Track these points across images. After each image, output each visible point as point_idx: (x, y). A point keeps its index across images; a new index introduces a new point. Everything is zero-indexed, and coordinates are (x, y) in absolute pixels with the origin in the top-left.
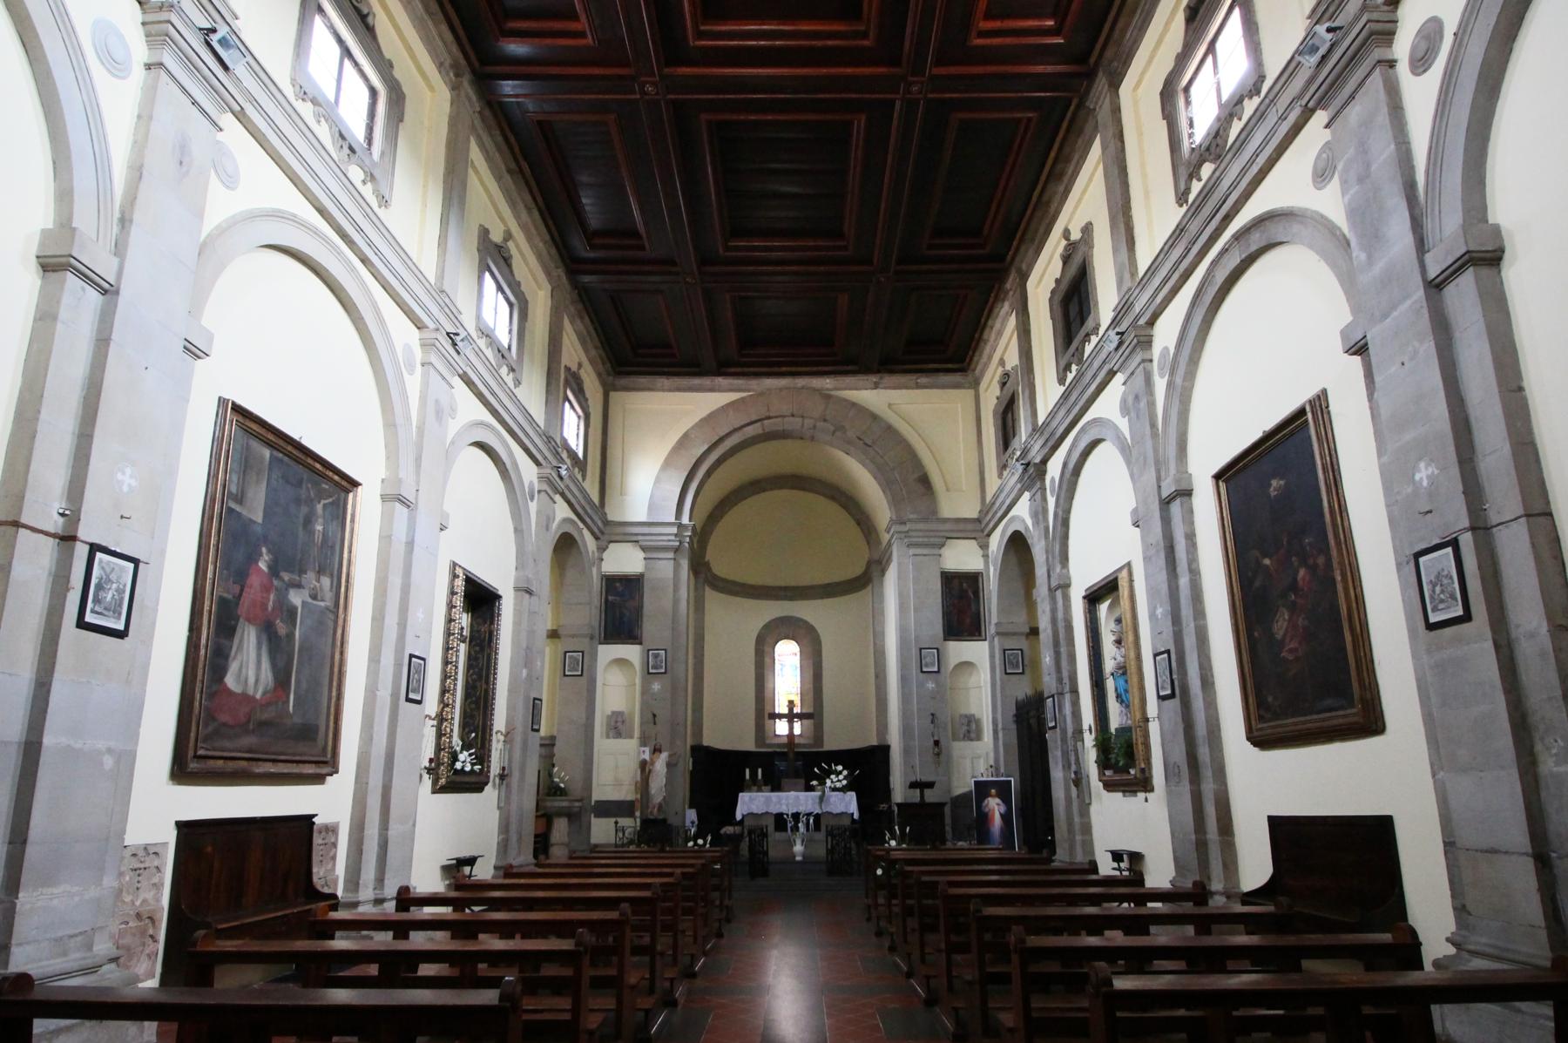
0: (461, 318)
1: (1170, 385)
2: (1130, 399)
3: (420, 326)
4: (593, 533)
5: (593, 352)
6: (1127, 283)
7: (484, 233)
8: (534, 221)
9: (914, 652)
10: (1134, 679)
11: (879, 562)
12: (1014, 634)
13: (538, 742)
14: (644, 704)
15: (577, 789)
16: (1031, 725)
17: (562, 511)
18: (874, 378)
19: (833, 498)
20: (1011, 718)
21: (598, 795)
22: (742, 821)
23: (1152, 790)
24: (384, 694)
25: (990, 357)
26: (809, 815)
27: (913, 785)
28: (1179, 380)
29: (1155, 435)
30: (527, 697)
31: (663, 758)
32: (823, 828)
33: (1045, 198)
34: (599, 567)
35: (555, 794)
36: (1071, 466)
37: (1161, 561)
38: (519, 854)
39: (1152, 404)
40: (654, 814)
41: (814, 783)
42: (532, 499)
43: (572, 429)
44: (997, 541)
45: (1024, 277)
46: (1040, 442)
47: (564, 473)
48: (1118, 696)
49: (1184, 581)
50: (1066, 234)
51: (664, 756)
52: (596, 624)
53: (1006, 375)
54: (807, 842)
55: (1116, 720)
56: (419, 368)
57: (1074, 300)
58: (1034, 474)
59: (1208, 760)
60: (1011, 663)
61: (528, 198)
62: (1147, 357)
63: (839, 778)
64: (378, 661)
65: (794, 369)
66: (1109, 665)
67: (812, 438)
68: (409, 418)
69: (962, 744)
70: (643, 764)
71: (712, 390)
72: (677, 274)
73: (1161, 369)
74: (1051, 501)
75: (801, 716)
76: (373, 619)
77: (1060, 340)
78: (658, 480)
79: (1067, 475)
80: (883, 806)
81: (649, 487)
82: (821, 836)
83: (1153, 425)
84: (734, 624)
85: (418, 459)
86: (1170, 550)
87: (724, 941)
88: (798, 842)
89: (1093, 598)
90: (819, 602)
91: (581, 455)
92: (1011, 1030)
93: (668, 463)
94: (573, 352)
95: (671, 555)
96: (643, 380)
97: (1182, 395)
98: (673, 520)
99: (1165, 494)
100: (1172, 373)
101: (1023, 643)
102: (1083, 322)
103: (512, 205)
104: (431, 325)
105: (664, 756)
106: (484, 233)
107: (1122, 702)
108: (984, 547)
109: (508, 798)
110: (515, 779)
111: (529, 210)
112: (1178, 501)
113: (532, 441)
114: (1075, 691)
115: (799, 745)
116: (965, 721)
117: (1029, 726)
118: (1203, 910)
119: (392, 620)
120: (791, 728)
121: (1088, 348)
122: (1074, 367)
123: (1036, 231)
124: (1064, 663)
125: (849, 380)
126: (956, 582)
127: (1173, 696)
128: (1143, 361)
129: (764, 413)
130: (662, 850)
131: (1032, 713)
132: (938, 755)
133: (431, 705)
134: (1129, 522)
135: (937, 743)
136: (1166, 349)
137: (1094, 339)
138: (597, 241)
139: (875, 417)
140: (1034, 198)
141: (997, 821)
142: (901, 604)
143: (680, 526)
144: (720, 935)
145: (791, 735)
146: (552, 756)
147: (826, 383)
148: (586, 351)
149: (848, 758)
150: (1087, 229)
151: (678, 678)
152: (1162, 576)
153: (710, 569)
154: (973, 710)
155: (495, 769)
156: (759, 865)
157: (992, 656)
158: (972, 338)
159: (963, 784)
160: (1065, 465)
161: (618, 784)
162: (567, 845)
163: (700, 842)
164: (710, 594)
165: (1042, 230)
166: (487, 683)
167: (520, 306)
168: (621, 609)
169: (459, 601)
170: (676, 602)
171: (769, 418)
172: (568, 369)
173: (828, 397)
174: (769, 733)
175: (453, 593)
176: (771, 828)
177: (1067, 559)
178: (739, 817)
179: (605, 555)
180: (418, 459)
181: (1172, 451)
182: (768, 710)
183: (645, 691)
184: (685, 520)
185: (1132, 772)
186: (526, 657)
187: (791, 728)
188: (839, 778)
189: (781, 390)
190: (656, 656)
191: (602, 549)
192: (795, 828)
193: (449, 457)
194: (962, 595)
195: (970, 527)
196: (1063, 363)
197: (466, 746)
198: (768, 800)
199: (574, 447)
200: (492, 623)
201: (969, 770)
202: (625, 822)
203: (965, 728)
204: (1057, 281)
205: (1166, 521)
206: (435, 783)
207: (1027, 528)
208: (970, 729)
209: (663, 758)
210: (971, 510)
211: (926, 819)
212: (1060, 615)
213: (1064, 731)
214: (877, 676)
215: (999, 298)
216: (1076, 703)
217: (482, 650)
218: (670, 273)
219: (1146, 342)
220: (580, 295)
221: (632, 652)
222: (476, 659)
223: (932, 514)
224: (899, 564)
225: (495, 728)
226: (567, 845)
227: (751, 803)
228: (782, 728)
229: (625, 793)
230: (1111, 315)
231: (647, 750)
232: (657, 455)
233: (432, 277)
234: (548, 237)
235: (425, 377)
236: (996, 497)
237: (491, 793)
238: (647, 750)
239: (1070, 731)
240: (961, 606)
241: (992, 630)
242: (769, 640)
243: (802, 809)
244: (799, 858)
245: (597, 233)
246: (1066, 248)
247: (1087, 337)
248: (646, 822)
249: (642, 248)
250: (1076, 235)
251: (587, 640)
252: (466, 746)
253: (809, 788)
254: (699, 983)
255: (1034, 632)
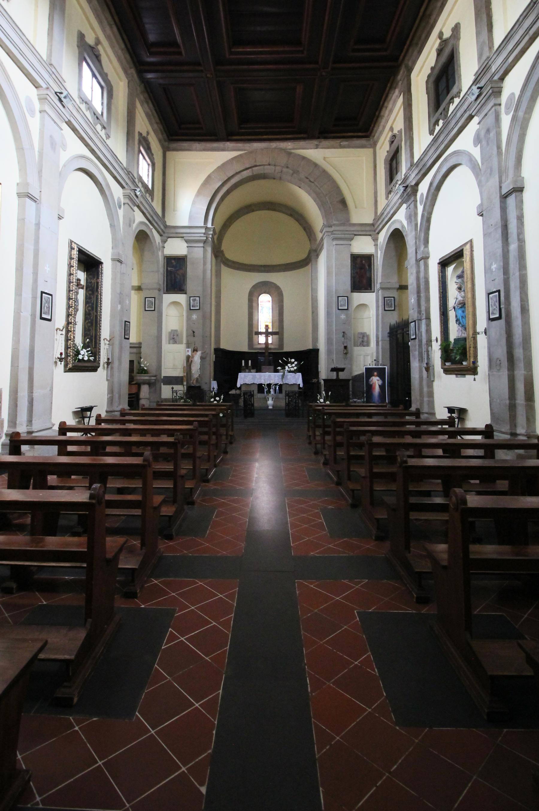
0: (66, 85)
1: (514, 119)
2: (483, 133)
3: (37, 86)
4: (158, 232)
5: (156, 126)
6: (486, 54)
7: (81, 36)
8: (113, 33)
9: (335, 299)
10: (469, 309)
11: (316, 251)
12: (389, 289)
13: (129, 346)
14: (188, 324)
15: (153, 371)
16: (399, 340)
17: (139, 217)
18: (315, 142)
19: (291, 215)
20: (386, 334)
21: (164, 374)
22: (240, 388)
23: (477, 374)
24: (26, 314)
25: (384, 127)
26: (276, 385)
27: (333, 370)
28: (521, 114)
29: (499, 153)
30: (121, 321)
31: (198, 354)
32: (284, 392)
33: (428, 12)
34: (163, 252)
35: (142, 373)
36: (435, 185)
37: (498, 234)
38: (119, 404)
39: (499, 134)
40: (194, 383)
41: (279, 368)
42: (120, 207)
43: (144, 170)
44: (383, 236)
45: (410, 70)
46: (416, 172)
47: (138, 193)
48: (457, 320)
49: (513, 247)
50: (441, 35)
51: (199, 353)
52: (161, 282)
53: (394, 136)
54: (275, 399)
55: (454, 332)
56: (38, 114)
57: (444, 78)
58: (411, 191)
59: (522, 357)
60: (388, 304)
61: (110, 18)
62: (497, 102)
63: (293, 365)
64: (21, 295)
65: (270, 137)
66: (451, 302)
67: (280, 178)
68: (32, 145)
69: (359, 348)
70: (188, 357)
71: (223, 150)
72: (202, 71)
73: (508, 108)
74: (420, 208)
75: (272, 333)
76: (17, 269)
77: (432, 105)
78: (194, 203)
79: (432, 190)
80: (315, 380)
81: (189, 206)
82: (282, 396)
83: (499, 147)
84: (236, 284)
85: (40, 172)
86: (505, 227)
87: (228, 456)
88: (270, 399)
89: (444, 264)
90: (282, 273)
91: (150, 186)
92: (364, 477)
93: (199, 193)
94: (143, 124)
95: (202, 245)
96: (185, 144)
97: (521, 125)
98: (202, 225)
99: (504, 191)
100: (516, 110)
101: (395, 294)
102: (448, 92)
103: (100, 22)
104: (44, 86)
105: (199, 353)
106: (81, 36)
107: (460, 323)
108: (375, 240)
109: (112, 375)
110: (116, 364)
111: (110, 26)
112: (514, 195)
113: (118, 173)
114: (428, 318)
115: (271, 349)
116: (361, 336)
117: (397, 339)
118: (418, 420)
119: (28, 270)
120: (267, 340)
121: (452, 108)
122: (441, 122)
123: (420, 38)
124: (423, 303)
125: (302, 143)
126: (359, 260)
127: (500, 318)
128: (495, 105)
129: (253, 164)
130: (194, 405)
131: (399, 332)
132: (346, 354)
133: (60, 320)
134: (476, 213)
135: (345, 347)
136: (513, 94)
137: (457, 101)
138: (154, 50)
139: (316, 165)
140: (421, 14)
141: (377, 390)
142: (328, 272)
143: (207, 228)
144: (226, 452)
145: (267, 343)
146: (140, 353)
147: (288, 145)
148: (151, 124)
149: (298, 355)
150: (456, 29)
151: (206, 312)
152: (498, 245)
153: (224, 255)
154: (366, 330)
155: (103, 358)
156: (249, 411)
157: (377, 301)
158: (379, 104)
159: (359, 369)
160: (431, 184)
161: (175, 368)
162: (149, 399)
163: (217, 399)
164: (224, 269)
165: (423, 36)
166: (97, 311)
167: (108, 89)
168: (175, 274)
169: (75, 263)
170: (204, 272)
171: (256, 166)
172: (140, 134)
173: (289, 154)
174: (255, 342)
175: (71, 258)
176: (256, 392)
177: (428, 242)
178: (238, 385)
179: (166, 245)
180: (40, 172)
181: (511, 163)
182: (255, 330)
183: (189, 318)
184: (209, 225)
185: (464, 363)
186: (120, 298)
187: (267, 340)
188: (293, 365)
189: (262, 149)
190: (194, 300)
191: (164, 242)
192: (269, 392)
193: (62, 176)
194: (362, 267)
195: (368, 228)
196: (433, 120)
197: (84, 347)
198: (254, 378)
199: (146, 182)
200: (98, 278)
201: (362, 363)
202: (177, 387)
203: (361, 340)
204: (432, 69)
205: (504, 209)
206: (66, 366)
207: (403, 226)
208: (364, 340)
209: (198, 354)
210: (369, 219)
211: (340, 387)
212: (422, 275)
213: (420, 341)
214: (313, 313)
215: (393, 87)
216: (428, 325)
217: (93, 293)
218: (198, 71)
219: (498, 92)
220: (145, 87)
221: (181, 298)
222: (90, 298)
223: (347, 221)
224: (328, 250)
225: (102, 337)
226: (149, 399)
227: (245, 378)
228: (262, 339)
229: (178, 373)
230: (473, 78)
231: (190, 350)
232: (194, 186)
233: (45, 57)
234: (123, 46)
235: (42, 120)
236: (382, 214)
237: (102, 372)
238: (190, 350)
239: (424, 341)
240: (361, 273)
241: (377, 286)
242: (256, 294)
243: (272, 382)
244: (270, 407)
245: (154, 44)
246: (440, 45)
247: (452, 100)
248: (190, 388)
249: (180, 53)
250: (447, 34)
251: (157, 291)
252: (84, 347)
253: (276, 371)
254: (211, 486)
255: (403, 288)
